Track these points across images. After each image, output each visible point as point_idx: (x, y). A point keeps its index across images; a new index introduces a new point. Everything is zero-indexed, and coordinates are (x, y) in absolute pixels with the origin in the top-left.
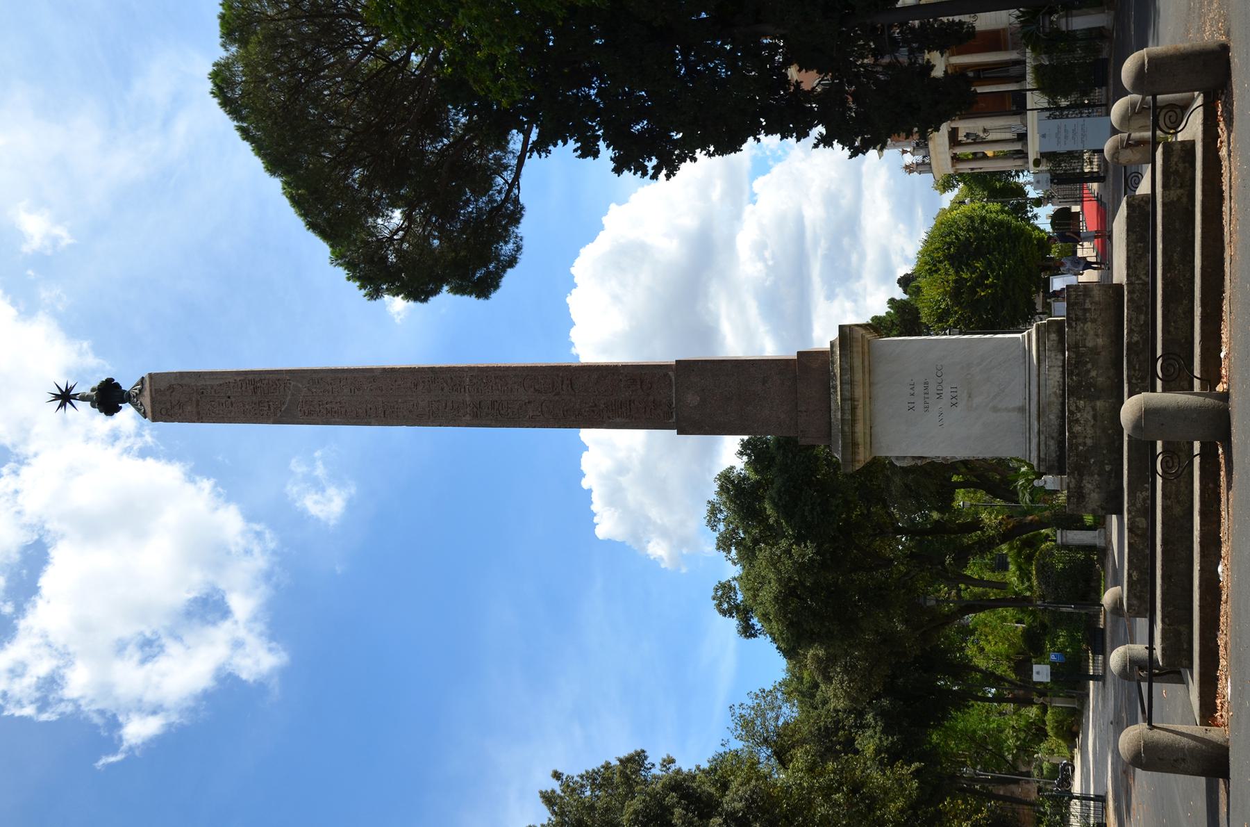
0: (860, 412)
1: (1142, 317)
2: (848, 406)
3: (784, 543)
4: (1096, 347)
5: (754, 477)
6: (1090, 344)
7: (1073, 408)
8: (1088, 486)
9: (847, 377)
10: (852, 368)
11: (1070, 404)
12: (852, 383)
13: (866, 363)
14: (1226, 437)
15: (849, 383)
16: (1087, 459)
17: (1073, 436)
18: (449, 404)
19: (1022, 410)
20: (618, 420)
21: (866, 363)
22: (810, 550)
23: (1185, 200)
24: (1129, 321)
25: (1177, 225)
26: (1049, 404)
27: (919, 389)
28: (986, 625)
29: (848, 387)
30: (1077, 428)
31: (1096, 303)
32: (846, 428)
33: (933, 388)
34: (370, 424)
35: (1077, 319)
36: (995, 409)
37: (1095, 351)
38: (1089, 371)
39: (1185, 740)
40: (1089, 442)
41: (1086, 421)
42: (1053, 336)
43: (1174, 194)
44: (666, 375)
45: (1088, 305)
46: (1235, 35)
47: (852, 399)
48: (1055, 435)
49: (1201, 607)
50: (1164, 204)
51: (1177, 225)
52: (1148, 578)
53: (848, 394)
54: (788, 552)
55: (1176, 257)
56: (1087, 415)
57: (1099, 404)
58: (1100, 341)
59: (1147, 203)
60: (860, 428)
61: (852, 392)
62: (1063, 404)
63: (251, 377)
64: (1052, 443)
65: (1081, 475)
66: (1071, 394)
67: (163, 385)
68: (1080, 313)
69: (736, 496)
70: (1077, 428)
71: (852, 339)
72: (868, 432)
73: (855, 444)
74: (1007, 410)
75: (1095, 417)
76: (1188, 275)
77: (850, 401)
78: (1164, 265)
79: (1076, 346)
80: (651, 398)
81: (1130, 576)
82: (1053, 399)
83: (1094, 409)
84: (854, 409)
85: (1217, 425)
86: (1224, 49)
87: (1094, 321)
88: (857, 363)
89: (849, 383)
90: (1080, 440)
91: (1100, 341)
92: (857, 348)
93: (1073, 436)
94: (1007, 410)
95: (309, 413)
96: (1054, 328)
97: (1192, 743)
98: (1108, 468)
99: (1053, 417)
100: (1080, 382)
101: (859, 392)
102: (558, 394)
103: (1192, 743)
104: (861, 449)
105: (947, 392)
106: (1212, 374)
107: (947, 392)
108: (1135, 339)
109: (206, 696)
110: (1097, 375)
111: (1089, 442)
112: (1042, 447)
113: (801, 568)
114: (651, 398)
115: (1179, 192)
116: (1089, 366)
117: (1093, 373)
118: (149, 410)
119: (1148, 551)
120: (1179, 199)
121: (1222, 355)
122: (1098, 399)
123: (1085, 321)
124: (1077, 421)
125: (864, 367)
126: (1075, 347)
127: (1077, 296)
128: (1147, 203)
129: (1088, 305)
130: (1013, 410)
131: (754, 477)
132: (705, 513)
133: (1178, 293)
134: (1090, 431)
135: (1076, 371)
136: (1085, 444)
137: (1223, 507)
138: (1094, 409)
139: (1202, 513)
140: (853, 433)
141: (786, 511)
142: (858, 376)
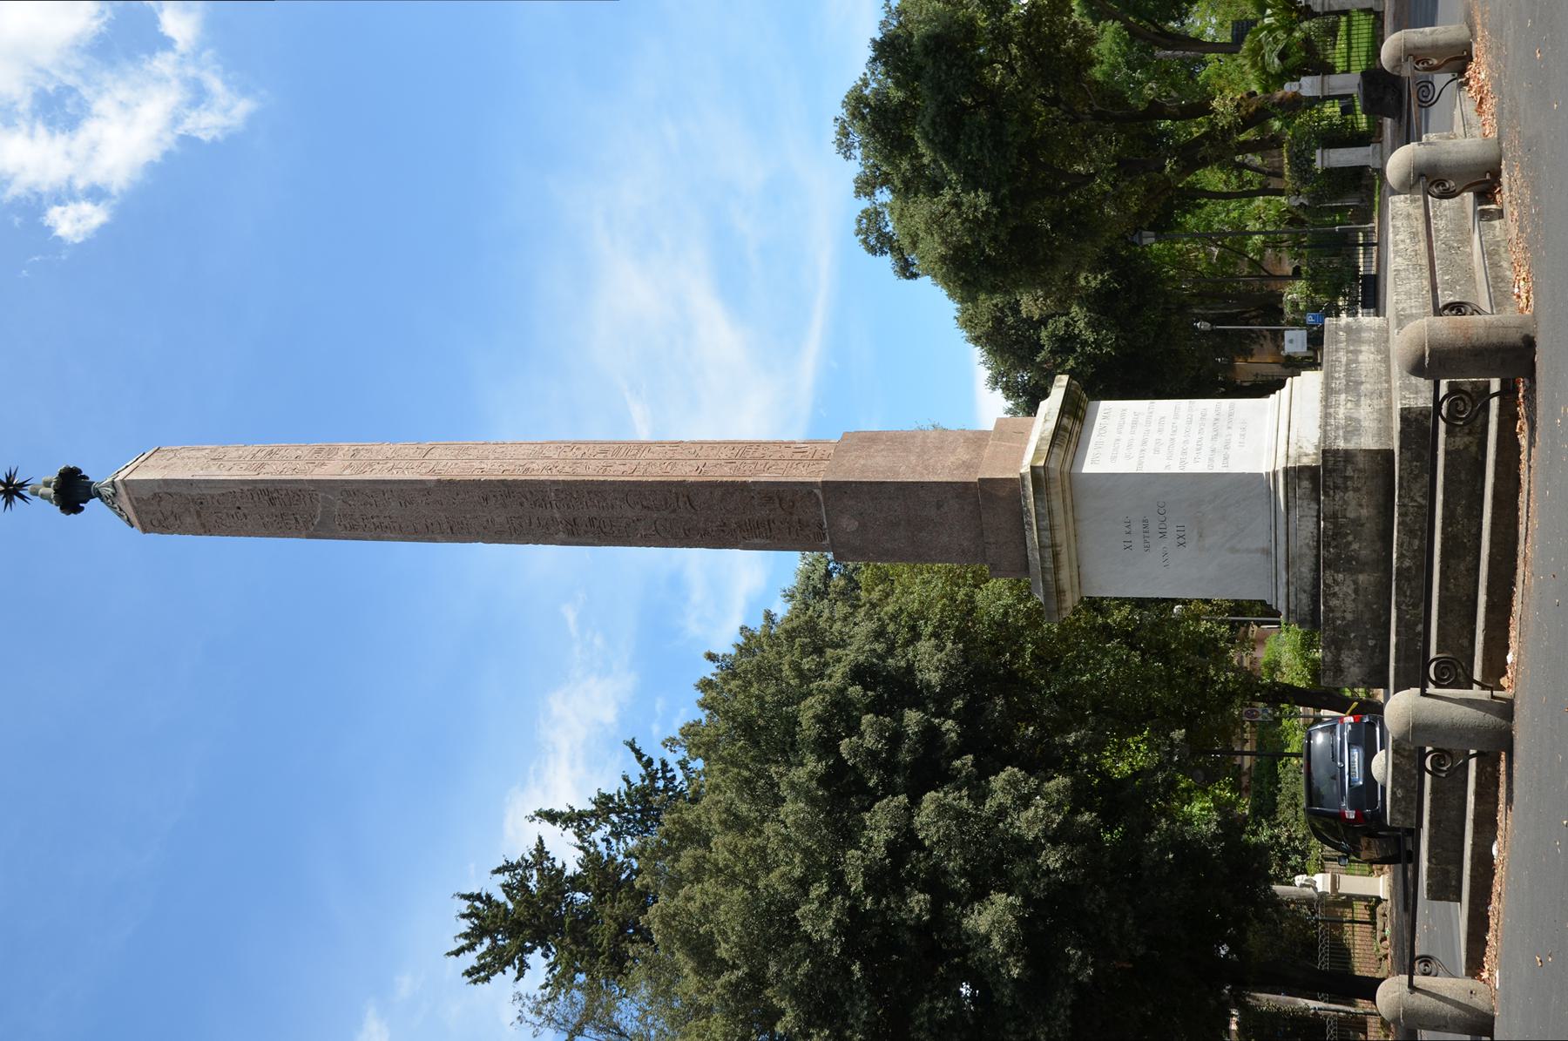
0: (1064, 558)
1: (1417, 542)
2: (1048, 553)
3: (947, 195)
4: (1359, 518)
5: (897, 95)
6: (1351, 514)
7: (1330, 581)
8: (1347, 659)
9: (1045, 523)
10: (1050, 512)
11: (1326, 576)
12: (1052, 528)
13: (1068, 501)
14: (1530, 373)
15: (1046, 514)
16: (1346, 633)
17: (1329, 609)
18: (534, 520)
19: (1267, 552)
20: (756, 541)
21: (1068, 501)
22: (983, 199)
23: (1473, 449)
24: (1400, 545)
25: (1463, 476)
26: (1300, 556)
27: (1137, 527)
28: (1220, 76)
29: (1047, 533)
30: (1334, 602)
31: (1360, 471)
32: (1048, 577)
33: (1154, 527)
34: (435, 541)
35: (1336, 487)
36: (1233, 550)
37: (1357, 523)
38: (1350, 543)
39: (1448, 1008)
40: (1349, 616)
41: (1346, 594)
42: (1306, 484)
43: (1460, 441)
44: (810, 493)
45: (1349, 472)
46: (1519, 695)
47: (1054, 545)
48: (1308, 588)
49: (1472, 877)
50: (1447, 453)
51: (1463, 476)
52: (1415, 796)
53: (1047, 542)
54: (956, 204)
55: (1459, 510)
56: (1348, 588)
57: (1361, 577)
58: (1364, 512)
59: (1427, 417)
60: (1064, 575)
61: (1053, 537)
62: (1318, 556)
63: (262, 486)
64: (1305, 598)
65: (1339, 650)
66: (1328, 566)
67: (146, 494)
68: (1339, 481)
69: (875, 124)
70: (1334, 602)
71: (1048, 480)
72: (1075, 573)
73: (1060, 592)
74: (1249, 551)
75: (1356, 591)
76: (1474, 531)
77: (1052, 551)
78: (1444, 518)
79: (1335, 516)
80: (795, 518)
81: (1393, 793)
82: (1305, 550)
83: (1355, 582)
84: (1056, 556)
85: (1496, 744)
86: (1529, 343)
87: (1357, 490)
88: (1057, 504)
89: (1046, 514)
90: (1338, 614)
91: (1364, 512)
92: (1055, 489)
93: (1329, 609)
94: (1249, 551)
95: (352, 528)
96: (1307, 475)
97: (1456, 1011)
98: (1371, 643)
99: (1306, 570)
100: (1338, 555)
101: (1061, 536)
102: (674, 511)
103: (1456, 1011)
104: (1068, 596)
105: (1172, 531)
106: (1496, 668)
107: (1172, 531)
108: (1407, 563)
109: (151, 168)
110: (1361, 548)
111: (1349, 616)
112: (1292, 598)
113: (976, 225)
114: (795, 518)
115: (1467, 439)
116: (1350, 538)
117: (1355, 546)
118: (134, 519)
119: (1420, 628)
120: (1467, 447)
121: (1510, 658)
122: (1361, 572)
123: (1346, 489)
124: (1335, 594)
125: (1065, 505)
126: (1333, 517)
127: (1336, 462)
128: (1427, 417)
129: (1349, 472)
130: (1257, 551)
131: (897, 95)
132: (833, 137)
133: (1461, 548)
134: (1350, 605)
135: (1333, 543)
136: (1344, 618)
137: (1524, 467)
138: (1355, 582)
139: (1478, 794)
140: (1057, 581)
141: (947, 149)
142: (1059, 519)
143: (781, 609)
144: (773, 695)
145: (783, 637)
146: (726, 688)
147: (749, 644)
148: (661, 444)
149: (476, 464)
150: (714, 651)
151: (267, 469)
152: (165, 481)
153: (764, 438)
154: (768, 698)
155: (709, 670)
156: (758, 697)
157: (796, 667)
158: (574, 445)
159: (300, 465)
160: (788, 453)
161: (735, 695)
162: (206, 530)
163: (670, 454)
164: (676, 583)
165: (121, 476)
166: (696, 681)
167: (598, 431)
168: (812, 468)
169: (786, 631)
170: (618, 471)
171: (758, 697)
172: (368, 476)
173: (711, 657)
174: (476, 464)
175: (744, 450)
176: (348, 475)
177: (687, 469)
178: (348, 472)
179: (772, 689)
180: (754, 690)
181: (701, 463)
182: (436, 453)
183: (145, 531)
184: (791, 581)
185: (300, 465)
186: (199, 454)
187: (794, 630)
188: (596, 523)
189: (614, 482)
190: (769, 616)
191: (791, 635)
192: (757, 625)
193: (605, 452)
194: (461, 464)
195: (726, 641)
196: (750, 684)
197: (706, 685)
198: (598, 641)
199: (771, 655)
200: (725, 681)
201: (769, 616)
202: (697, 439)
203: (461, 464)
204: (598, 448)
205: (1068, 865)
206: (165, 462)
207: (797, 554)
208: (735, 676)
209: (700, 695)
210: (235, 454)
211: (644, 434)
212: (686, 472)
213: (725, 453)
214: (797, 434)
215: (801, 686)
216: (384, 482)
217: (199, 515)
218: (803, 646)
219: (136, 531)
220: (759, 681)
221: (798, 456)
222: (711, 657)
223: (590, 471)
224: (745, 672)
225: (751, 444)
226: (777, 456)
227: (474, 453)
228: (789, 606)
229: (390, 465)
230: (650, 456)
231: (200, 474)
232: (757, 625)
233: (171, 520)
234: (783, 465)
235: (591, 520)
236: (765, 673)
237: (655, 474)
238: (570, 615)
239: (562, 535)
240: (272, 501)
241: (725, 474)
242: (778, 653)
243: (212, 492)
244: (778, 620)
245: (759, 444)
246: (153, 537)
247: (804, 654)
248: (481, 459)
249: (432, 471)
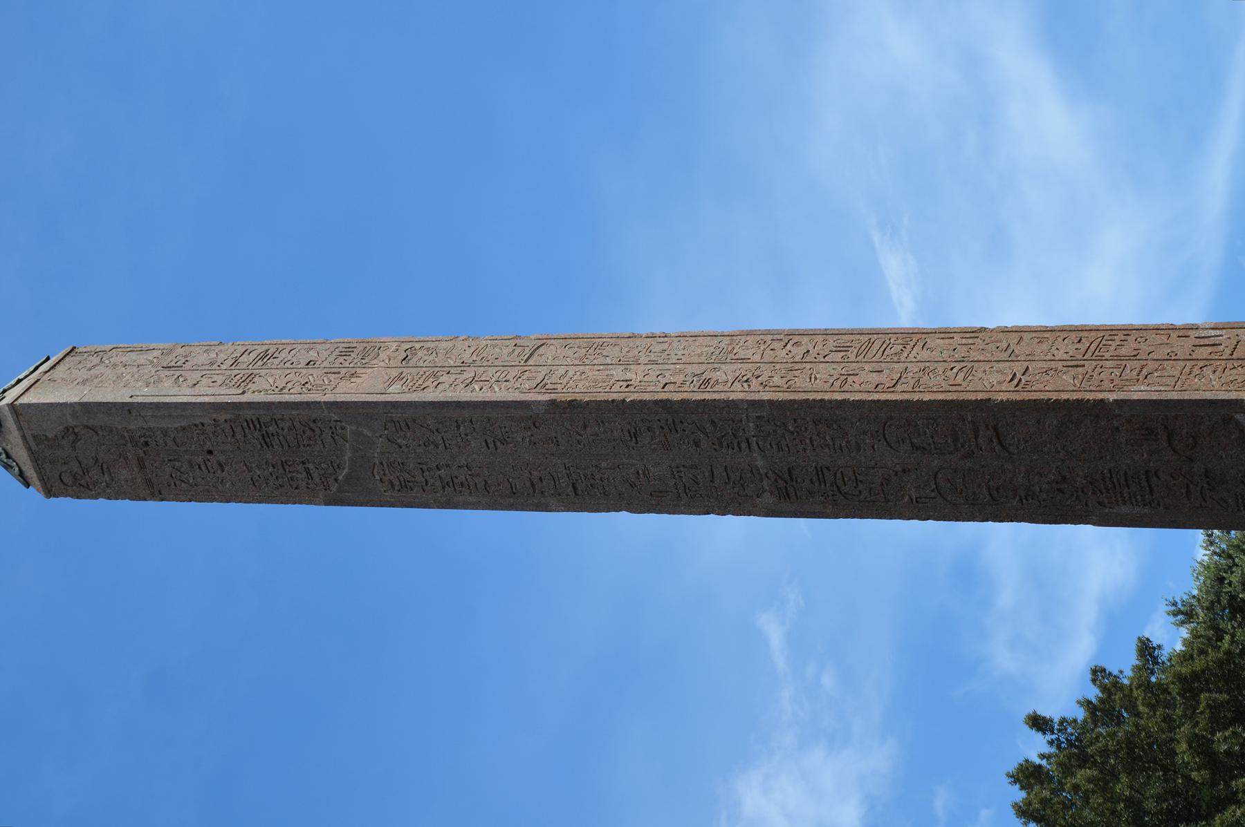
20: (1125, 509)
34: (546, 508)
63: (249, 414)
70: (1107, 385)
95: (404, 486)
102: (970, 455)
118: (30, 473)
143: (1172, 639)
144: (1159, 799)
145: (1174, 690)
146: (1069, 782)
147: (1109, 698)
148: (946, 333)
149: (618, 373)
150: (1045, 712)
151: (260, 383)
152: (85, 407)
153: (1137, 321)
154: (1150, 805)
155: (1036, 747)
156: (1129, 801)
157: (1201, 746)
158: (790, 337)
159: (314, 376)
160: (1182, 348)
161: (1086, 799)
162: (154, 491)
163: (962, 352)
164: (969, 574)
165: (9, 397)
166: (1012, 767)
167: (820, 310)
168: (1230, 375)
169: (1180, 678)
170: (868, 383)
171: (1129, 801)
172: (430, 395)
173: (1038, 723)
174: (618, 373)
175: (1098, 342)
176: (397, 394)
177: (994, 379)
178: (396, 387)
179: (1156, 789)
180: (1122, 787)
181: (1018, 368)
182: (548, 353)
183: (49, 492)
184: (1188, 586)
185: (314, 376)
186: (142, 359)
187: (1195, 676)
188: (829, 477)
189: (860, 404)
190: (1146, 650)
191: (1191, 684)
192: (1124, 664)
193: (844, 349)
194: (591, 373)
195: (1064, 693)
196: (1115, 777)
197: (1027, 775)
198: (828, 680)
199: (1153, 724)
200: (1066, 769)
201: (1146, 650)
202: (1010, 322)
203: (591, 373)
204: (831, 343)
205: (1228, 753)
206: (83, 374)
207: (1199, 535)
208: (1084, 760)
209: (1018, 795)
210: (203, 359)
211: (906, 317)
212: (992, 383)
213: (1064, 350)
214: (1191, 310)
215: (1214, 784)
216: (459, 405)
217: (141, 464)
218: (1214, 707)
219: (34, 495)
220: (1131, 772)
221: (1204, 352)
222: (1038, 723)
223: (818, 384)
224: (1104, 752)
225: (1113, 331)
226: (1163, 352)
227: (613, 353)
228: (1184, 632)
229: (469, 374)
230: (925, 355)
231: (144, 393)
232: (1124, 664)
233: (95, 472)
234: (1174, 369)
235: (820, 471)
236: (1141, 756)
237: (936, 386)
238: (774, 631)
239: (767, 499)
240: (266, 440)
241: (1064, 386)
242: (1167, 719)
243: (164, 424)
244: (1164, 655)
245: (1127, 331)
246: (65, 504)
247: (1217, 723)
248: (625, 364)
249: (542, 385)
